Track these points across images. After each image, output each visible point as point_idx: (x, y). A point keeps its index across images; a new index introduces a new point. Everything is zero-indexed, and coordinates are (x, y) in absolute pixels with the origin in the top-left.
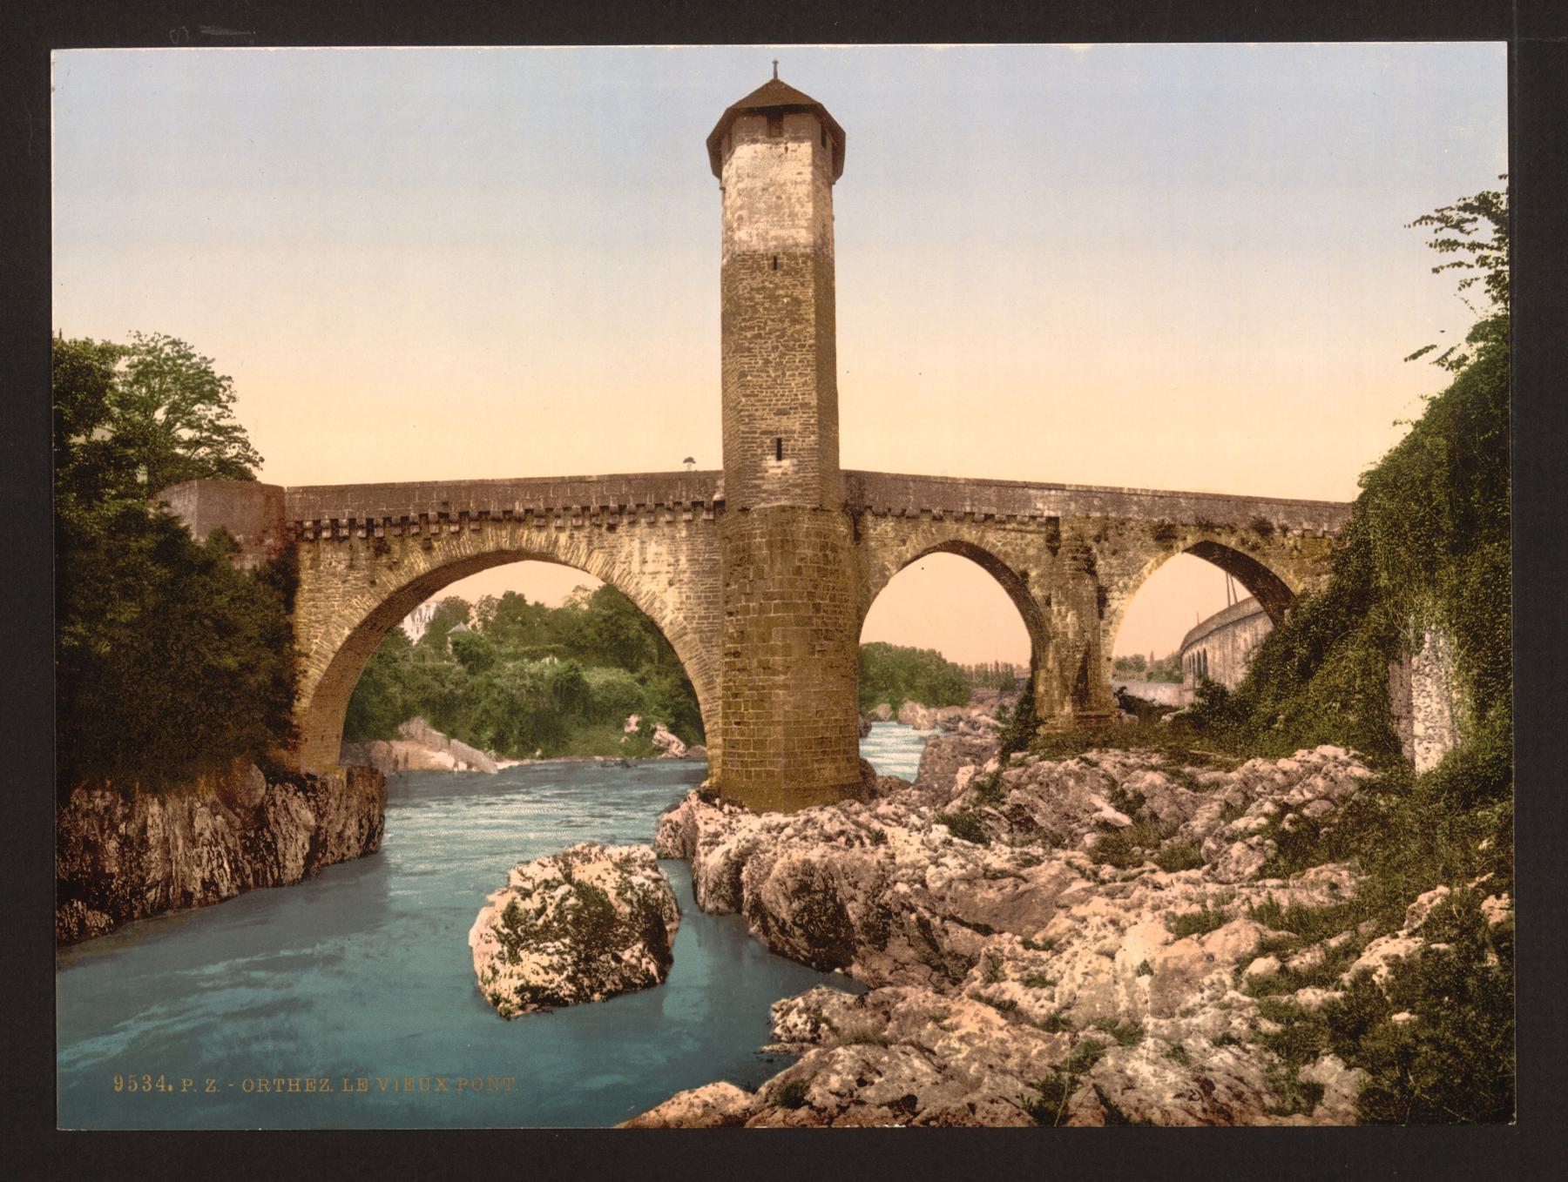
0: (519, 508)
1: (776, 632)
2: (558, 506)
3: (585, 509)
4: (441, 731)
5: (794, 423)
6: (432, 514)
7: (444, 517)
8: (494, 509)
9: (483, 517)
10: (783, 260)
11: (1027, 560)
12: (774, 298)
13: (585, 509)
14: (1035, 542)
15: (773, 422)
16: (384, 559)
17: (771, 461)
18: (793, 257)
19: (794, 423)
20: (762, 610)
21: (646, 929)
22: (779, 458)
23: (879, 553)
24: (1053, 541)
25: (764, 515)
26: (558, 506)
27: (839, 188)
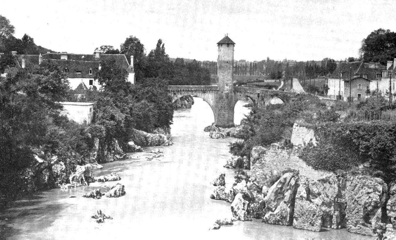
0: (193, 90)
1: (226, 107)
2: (198, 90)
3: (201, 90)
4: (379, 177)
5: (229, 82)
6: (182, 90)
7: (183, 91)
8: (190, 90)
9: (189, 91)
10: (228, 62)
11: (255, 98)
12: (227, 67)
13: (201, 90)
14: (256, 96)
15: (226, 82)
16: (175, 95)
17: (226, 87)
18: (230, 62)
19: (229, 82)
20: (224, 104)
21: (33, 175)
22: (227, 86)
23: (239, 169)
24: (258, 96)
25: (225, 93)
26: (198, 90)
27: (234, 47)
